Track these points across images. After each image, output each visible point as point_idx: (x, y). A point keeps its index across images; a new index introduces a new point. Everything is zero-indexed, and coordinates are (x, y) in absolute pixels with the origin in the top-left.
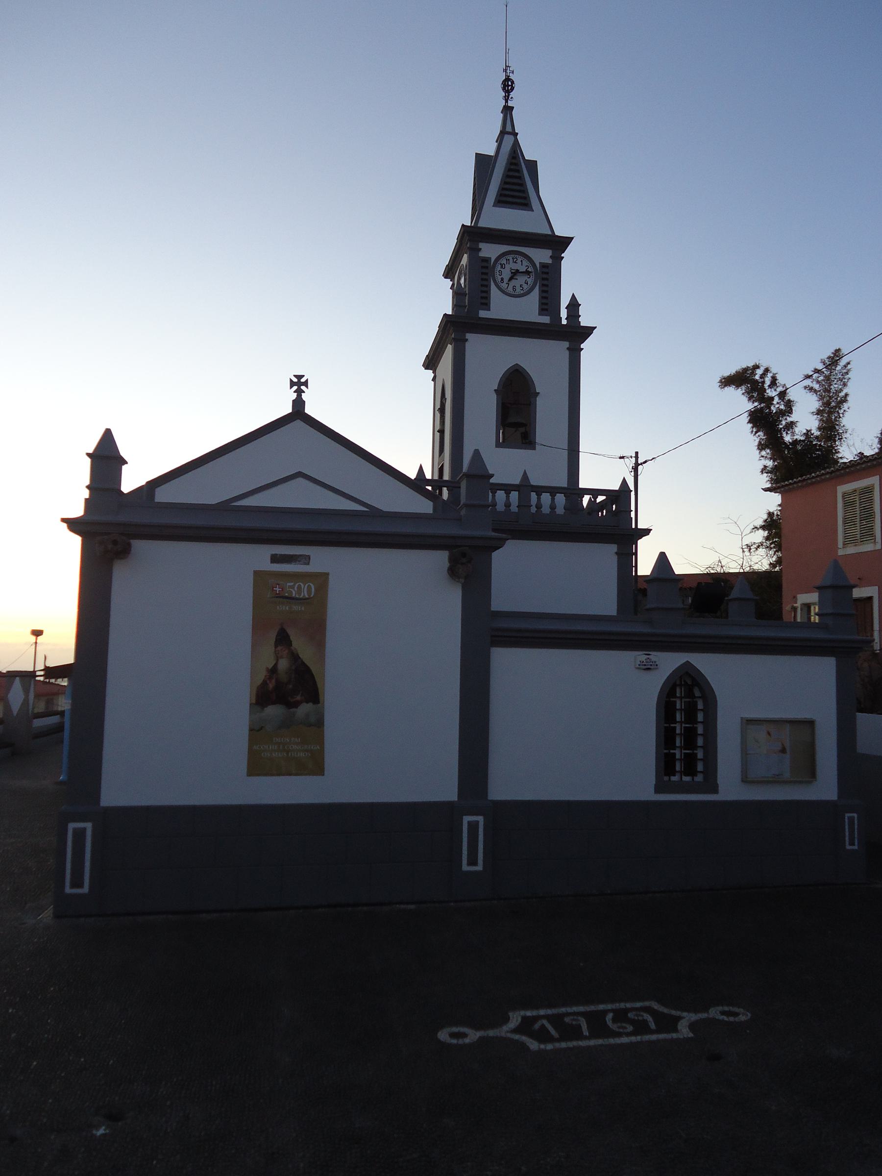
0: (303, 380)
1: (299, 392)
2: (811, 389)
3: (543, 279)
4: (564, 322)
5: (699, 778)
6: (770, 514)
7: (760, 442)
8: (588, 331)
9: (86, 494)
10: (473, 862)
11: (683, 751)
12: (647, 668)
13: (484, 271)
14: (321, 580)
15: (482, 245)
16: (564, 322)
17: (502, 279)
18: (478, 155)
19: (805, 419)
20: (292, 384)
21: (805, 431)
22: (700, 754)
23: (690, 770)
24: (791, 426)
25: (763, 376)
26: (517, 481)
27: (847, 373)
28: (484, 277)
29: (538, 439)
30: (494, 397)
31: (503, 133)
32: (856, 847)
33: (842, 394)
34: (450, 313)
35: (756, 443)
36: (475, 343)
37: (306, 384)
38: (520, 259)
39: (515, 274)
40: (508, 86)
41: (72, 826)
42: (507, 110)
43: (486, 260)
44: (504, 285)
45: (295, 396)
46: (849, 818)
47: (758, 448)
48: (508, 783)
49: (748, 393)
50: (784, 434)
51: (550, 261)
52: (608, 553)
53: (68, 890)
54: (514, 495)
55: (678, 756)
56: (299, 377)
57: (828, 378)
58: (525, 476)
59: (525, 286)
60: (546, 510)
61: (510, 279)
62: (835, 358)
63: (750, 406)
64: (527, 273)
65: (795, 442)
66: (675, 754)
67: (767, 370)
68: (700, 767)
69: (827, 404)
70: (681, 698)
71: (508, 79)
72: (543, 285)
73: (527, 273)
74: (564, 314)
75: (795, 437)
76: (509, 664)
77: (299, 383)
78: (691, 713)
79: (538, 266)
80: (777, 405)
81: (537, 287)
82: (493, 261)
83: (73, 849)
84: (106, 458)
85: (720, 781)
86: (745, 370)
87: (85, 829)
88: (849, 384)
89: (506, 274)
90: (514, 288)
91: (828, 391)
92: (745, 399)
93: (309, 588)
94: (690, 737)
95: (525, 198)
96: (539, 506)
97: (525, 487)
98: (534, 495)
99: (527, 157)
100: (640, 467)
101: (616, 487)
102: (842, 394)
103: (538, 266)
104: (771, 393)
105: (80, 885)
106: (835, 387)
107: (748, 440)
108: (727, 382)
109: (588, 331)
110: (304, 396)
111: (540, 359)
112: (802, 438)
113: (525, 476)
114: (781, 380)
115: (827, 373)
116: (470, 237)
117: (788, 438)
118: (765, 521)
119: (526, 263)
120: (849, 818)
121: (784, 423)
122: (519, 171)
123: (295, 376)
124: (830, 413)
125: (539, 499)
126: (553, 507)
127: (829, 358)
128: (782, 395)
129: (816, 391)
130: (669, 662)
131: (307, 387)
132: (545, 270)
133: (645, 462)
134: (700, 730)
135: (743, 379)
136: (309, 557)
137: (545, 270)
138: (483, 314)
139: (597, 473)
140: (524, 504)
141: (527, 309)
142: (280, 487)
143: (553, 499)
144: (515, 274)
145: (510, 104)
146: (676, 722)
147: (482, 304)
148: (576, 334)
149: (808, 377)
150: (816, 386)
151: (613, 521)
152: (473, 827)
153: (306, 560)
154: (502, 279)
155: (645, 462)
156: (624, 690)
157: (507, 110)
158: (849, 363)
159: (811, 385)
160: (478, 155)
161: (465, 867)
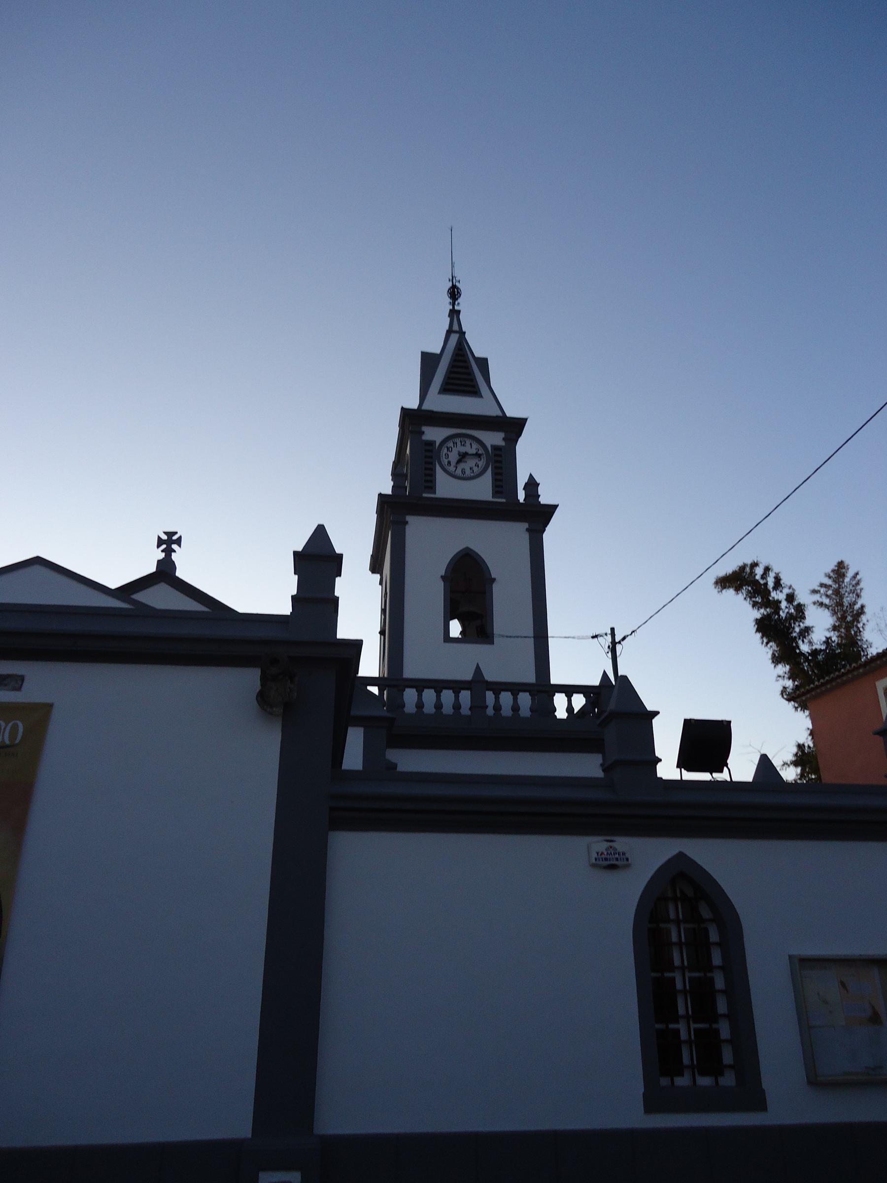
0: (165, 537)
1: (169, 552)
2: (821, 604)
3: (496, 462)
5: (728, 1080)
6: (800, 747)
7: (773, 654)
8: (551, 509)
11: (693, 1026)
12: (612, 864)
14: (39, 716)
15: (424, 429)
17: (449, 463)
18: (422, 353)
19: (820, 626)
20: (160, 542)
21: (824, 639)
22: (725, 1030)
23: (710, 1063)
24: (807, 630)
25: (763, 577)
26: (468, 676)
27: (858, 583)
29: (496, 631)
30: (441, 584)
31: (449, 332)
33: (857, 607)
34: (388, 491)
35: (770, 656)
37: (179, 542)
38: (468, 442)
39: (463, 457)
40: (454, 293)
42: (454, 314)
43: (431, 443)
44: (451, 469)
45: (163, 555)
47: (773, 662)
49: (751, 598)
50: (800, 642)
51: (503, 443)
54: (465, 696)
55: (684, 1036)
56: (170, 534)
57: (837, 592)
58: (478, 670)
59: (475, 469)
60: (506, 711)
61: (459, 461)
62: (840, 570)
63: (757, 614)
64: (477, 455)
65: (815, 653)
66: (677, 1031)
67: (767, 569)
68: (728, 1056)
69: (843, 619)
70: (678, 922)
71: (454, 287)
72: (496, 468)
73: (477, 455)
74: (521, 496)
75: (814, 648)
76: (369, 867)
78: (698, 946)
79: (490, 449)
80: (785, 609)
82: (437, 444)
86: (743, 568)
88: (862, 594)
89: (454, 457)
90: (463, 471)
91: (840, 604)
92: (747, 605)
93: (15, 728)
94: (703, 995)
96: (497, 707)
97: (478, 684)
98: (490, 695)
99: (478, 354)
100: (618, 647)
101: (596, 682)
102: (857, 607)
103: (490, 449)
104: (775, 595)
106: (846, 601)
107: (761, 652)
108: (724, 582)
109: (551, 509)
110: (174, 556)
111: (497, 544)
112: (823, 647)
113: (478, 670)
114: (785, 581)
115: (835, 586)
116: (411, 420)
117: (805, 648)
118: (796, 755)
119: (475, 446)
121: (797, 630)
122: (468, 367)
123: (165, 533)
124: (848, 629)
125: (497, 698)
126: (516, 708)
127: (833, 571)
128: (790, 598)
129: (827, 607)
130: (650, 854)
132: (498, 452)
133: (624, 638)
134: (720, 982)
135: (740, 580)
136: (22, 678)
137: (498, 452)
139: (575, 663)
140: (478, 705)
141: (481, 489)
144: (463, 457)
145: (456, 308)
146: (672, 968)
147: (426, 487)
148: (538, 516)
149: (815, 592)
150: (826, 601)
153: (17, 682)
154: (449, 463)
155: (624, 638)
156: (575, 904)
157: (454, 314)
158: (857, 574)
159: (820, 600)
160: (422, 353)
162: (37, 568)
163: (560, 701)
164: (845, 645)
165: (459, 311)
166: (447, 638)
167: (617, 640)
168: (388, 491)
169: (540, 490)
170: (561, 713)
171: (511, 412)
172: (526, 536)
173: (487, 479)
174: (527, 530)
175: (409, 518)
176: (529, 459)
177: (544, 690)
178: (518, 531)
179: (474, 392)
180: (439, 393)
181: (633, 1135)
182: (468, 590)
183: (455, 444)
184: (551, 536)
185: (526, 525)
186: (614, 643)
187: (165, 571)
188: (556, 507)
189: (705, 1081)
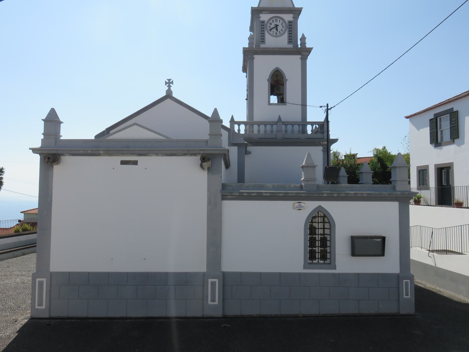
0: (167, 81)
1: (169, 87)
4: (299, 46)
5: (328, 261)
9: (42, 137)
13: (263, 27)
15: (261, 15)
16: (299, 46)
20: (166, 83)
22: (328, 249)
23: (324, 257)
28: (263, 29)
30: (267, 82)
32: (409, 297)
34: (247, 46)
36: (258, 59)
37: (172, 83)
41: (38, 280)
43: (263, 22)
45: (167, 88)
46: (405, 282)
48: (232, 263)
51: (292, 19)
52: (316, 153)
53: (37, 307)
56: (169, 80)
74: (299, 43)
76: (233, 209)
77: (169, 83)
81: (287, 32)
83: (43, 290)
84: (52, 121)
85: (337, 263)
87: (43, 281)
94: (324, 241)
100: (329, 111)
111: (288, 64)
113: (280, 118)
120: (405, 282)
130: (310, 206)
131: (173, 84)
132: (290, 24)
133: (331, 108)
137: (290, 24)
138: (262, 46)
139: (315, 115)
141: (282, 41)
142: (413, 113)
148: (304, 52)
151: (322, 136)
152: (213, 284)
155: (331, 108)
162: (135, 126)
163: (309, 129)
164: (352, 167)
166: (269, 104)
167: (329, 108)
168: (247, 46)
170: (309, 132)
171: (297, 5)
173: (286, 36)
174: (301, 59)
175: (255, 56)
176: (303, 27)
177: (304, 123)
181: (300, 274)
182: (277, 85)
184: (310, 60)
185: (300, 56)
186: (328, 110)
187: (169, 95)
188: (312, 48)
189: (322, 262)
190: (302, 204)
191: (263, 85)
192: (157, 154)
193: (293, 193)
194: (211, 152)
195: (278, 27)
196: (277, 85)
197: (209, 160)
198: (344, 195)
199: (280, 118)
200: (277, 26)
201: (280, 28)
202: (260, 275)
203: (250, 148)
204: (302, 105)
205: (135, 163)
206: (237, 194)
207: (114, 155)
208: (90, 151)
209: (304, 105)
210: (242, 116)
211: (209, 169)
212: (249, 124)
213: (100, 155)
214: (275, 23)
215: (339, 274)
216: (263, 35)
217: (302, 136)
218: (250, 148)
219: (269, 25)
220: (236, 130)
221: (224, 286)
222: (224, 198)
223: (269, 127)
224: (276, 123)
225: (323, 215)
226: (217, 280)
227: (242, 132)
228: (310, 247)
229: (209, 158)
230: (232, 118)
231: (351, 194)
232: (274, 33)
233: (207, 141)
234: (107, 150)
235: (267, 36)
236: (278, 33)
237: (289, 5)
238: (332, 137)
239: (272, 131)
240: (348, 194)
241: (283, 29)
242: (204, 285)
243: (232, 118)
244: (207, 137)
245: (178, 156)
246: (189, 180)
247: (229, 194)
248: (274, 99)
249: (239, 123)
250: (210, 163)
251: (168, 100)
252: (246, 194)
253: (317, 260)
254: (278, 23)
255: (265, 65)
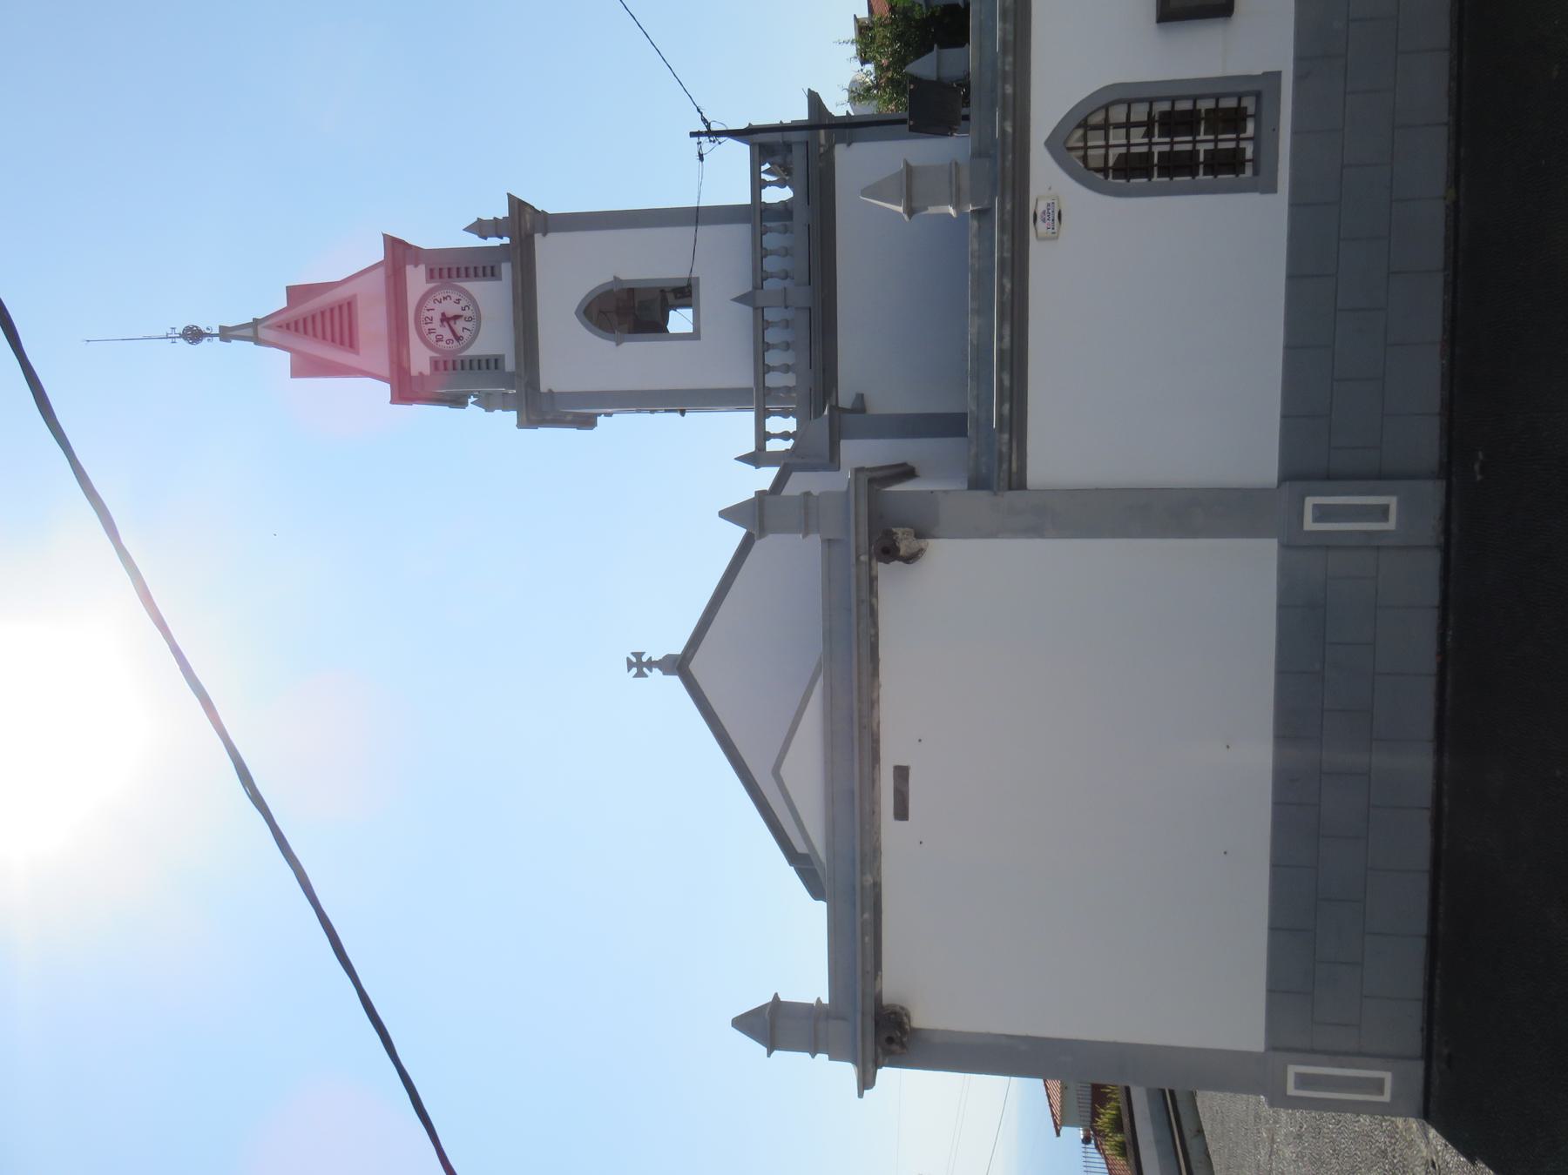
0: (634, 670)
1: (651, 664)
4: (506, 240)
5: (1249, 104)
8: (517, 205)
10: (1383, 513)
15: (414, 372)
20: (640, 674)
23: (1233, 120)
26: (747, 311)
30: (626, 345)
31: (257, 340)
36: (554, 376)
37: (639, 655)
40: (194, 335)
42: (226, 334)
43: (435, 364)
45: (656, 671)
56: (630, 665)
59: (463, 303)
71: (184, 335)
74: (494, 242)
77: (639, 665)
84: (773, 1025)
95: (340, 307)
100: (714, 127)
103: (431, 285)
105: (1381, 1082)
110: (656, 657)
111: (567, 274)
113: (741, 299)
116: (406, 390)
130: (1047, 178)
133: (704, 120)
137: (436, 273)
138: (509, 365)
139: (728, 178)
141: (492, 297)
143: (772, 253)
145: (216, 331)
146: (1150, 154)
148: (524, 225)
152: (1323, 514)
155: (704, 120)
157: (226, 334)
161: (1391, 525)
163: (775, 195)
165: (221, 328)
166: (695, 335)
169: (488, 216)
170: (786, 194)
171: (378, 254)
172: (551, 236)
173: (475, 287)
175: (544, 388)
176: (444, 229)
177: (757, 214)
178: (545, 246)
179: (348, 306)
180: (357, 353)
182: (631, 311)
183: (430, 331)
184: (548, 202)
185: (538, 237)
186: (710, 133)
187: (678, 665)
188: (509, 195)
190: (1042, 207)
191: (633, 360)
192: (873, 703)
193: (1001, 242)
194: (864, 529)
195: (450, 314)
196: (631, 311)
197: (889, 534)
198: (1010, 59)
199: (741, 299)
200: (445, 319)
201: (451, 309)
202: (1294, 347)
203: (845, 398)
204: (697, 223)
205: (902, 773)
206: (1006, 436)
207: (878, 839)
208: (866, 916)
209: (697, 216)
210: (738, 427)
211: (920, 535)
212: (762, 401)
213: (877, 886)
214: (436, 323)
215: (1299, 59)
216: (475, 364)
217: (801, 217)
218: (845, 398)
219: (443, 344)
220: (788, 444)
221: (1329, 477)
222: (1017, 481)
223: (772, 336)
224: (759, 311)
225: (1080, 132)
226: (1310, 502)
227: (790, 424)
228: (1194, 174)
229: (885, 535)
230: (745, 459)
231: (1004, 31)
232: (469, 325)
233: (828, 542)
234: (862, 862)
235: (479, 349)
236: (468, 313)
237: (379, 281)
238: (801, 113)
239: (787, 324)
240: (1004, 42)
241: (455, 297)
242: (1325, 544)
243: (745, 459)
244: (815, 540)
245: (877, 635)
246: (960, 598)
247: (1005, 466)
248: (680, 321)
249: (762, 436)
250: (899, 531)
251: (694, 667)
252: (1006, 407)
253: (1243, 144)
254: (437, 317)
255: (572, 354)
